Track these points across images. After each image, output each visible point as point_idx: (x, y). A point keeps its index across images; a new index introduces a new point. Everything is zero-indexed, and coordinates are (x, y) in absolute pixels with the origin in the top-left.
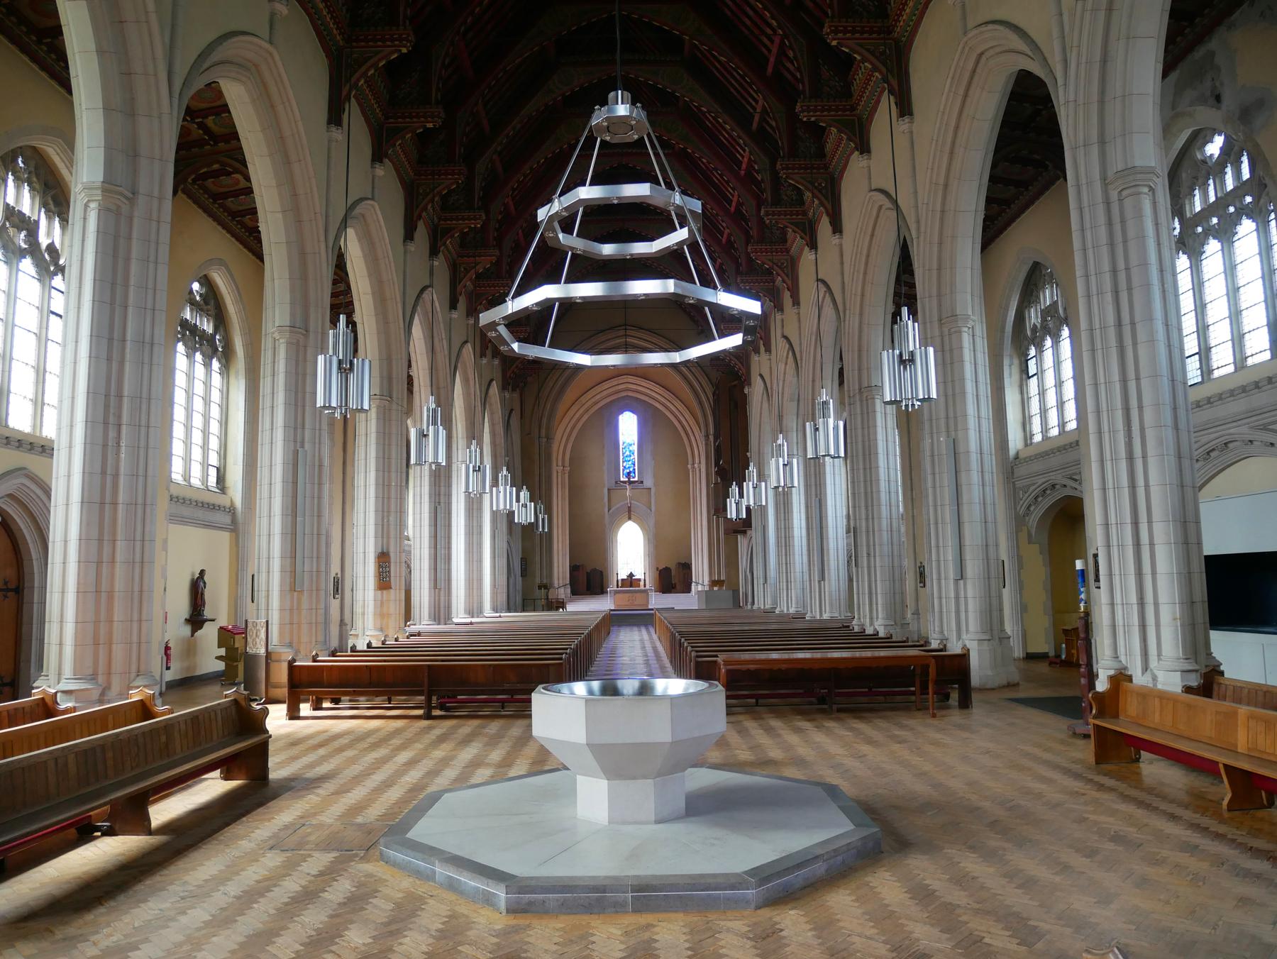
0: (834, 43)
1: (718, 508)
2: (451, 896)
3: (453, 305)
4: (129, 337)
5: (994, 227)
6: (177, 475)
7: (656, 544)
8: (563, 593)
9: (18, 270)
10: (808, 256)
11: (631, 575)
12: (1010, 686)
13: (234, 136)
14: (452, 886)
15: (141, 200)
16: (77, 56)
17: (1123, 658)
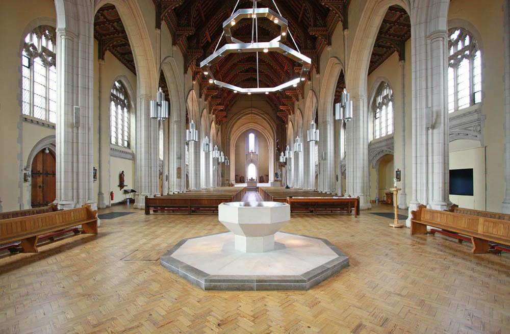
0: (323, 4)
1: (277, 158)
2: (184, 281)
3: (200, 97)
4: (79, 86)
5: (374, 65)
6: (113, 141)
7: (259, 169)
8: (233, 182)
10: (297, 103)
11: (252, 178)
12: (369, 209)
13: (119, 20)
14: (185, 277)
15: (81, 37)
17: (419, 201)
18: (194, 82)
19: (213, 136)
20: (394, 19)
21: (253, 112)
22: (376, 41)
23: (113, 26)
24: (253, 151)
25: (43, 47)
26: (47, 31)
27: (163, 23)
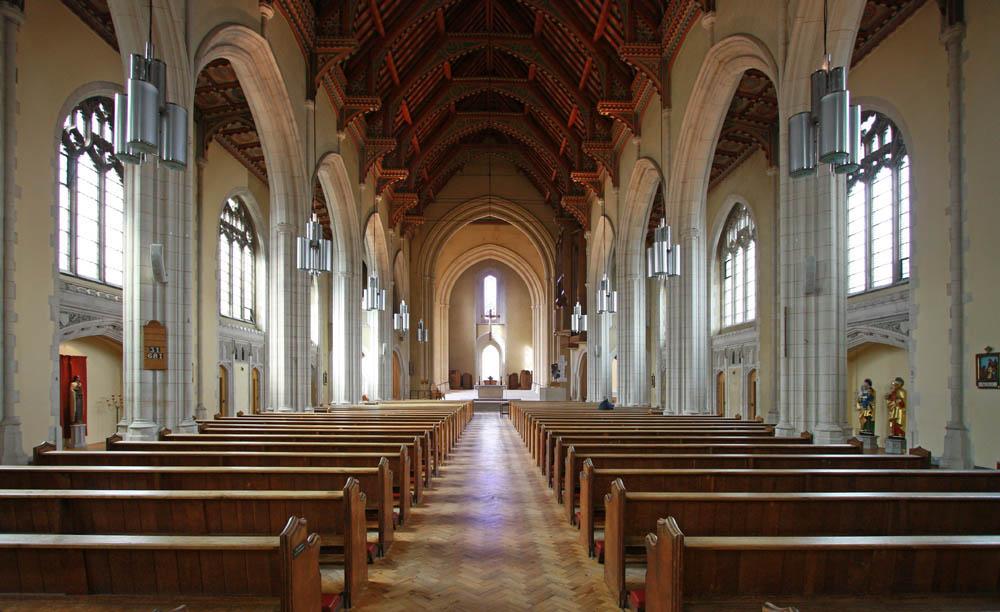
5: (721, 168)
8: (443, 388)
9: (105, 177)
11: (490, 378)
16: (274, 174)
18: (380, 199)
19: (380, 260)
20: (759, 89)
21: (493, 207)
22: (722, 132)
23: (224, 95)
24: (494, 313)
25: (94, 136)
26: (101, 106)
27: (321, 92)
